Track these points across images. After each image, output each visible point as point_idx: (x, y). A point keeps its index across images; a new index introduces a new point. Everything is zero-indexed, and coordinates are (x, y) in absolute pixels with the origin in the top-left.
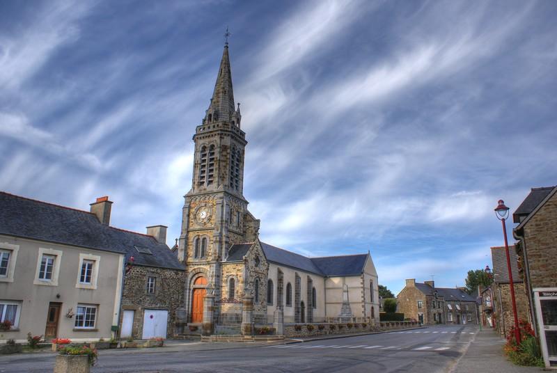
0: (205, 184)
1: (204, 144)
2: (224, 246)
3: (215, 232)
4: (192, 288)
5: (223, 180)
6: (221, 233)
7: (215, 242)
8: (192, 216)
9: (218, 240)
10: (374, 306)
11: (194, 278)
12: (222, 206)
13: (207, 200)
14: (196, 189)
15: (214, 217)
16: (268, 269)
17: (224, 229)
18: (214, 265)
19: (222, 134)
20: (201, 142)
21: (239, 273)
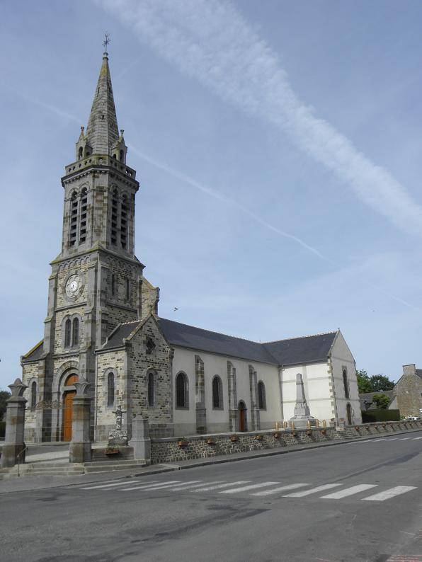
0: (76, 243)
1: (74, 189)
2: (99, 327)
3: (88, 308)
4: (62, 392)
5: (99, 235)
6: (94, 310)
7: (87, 322)
8: (60, 290)
9: (90, 318)
10: (351, 403)
11: (65, 377)
12: (96, 271)
13: (78, 266)
14: (65, 251)
15: (86, 288)
16: (172, 357)
17: (98, 303)
18: (85, 355)
19: (95, 172)
20: (70, 187)
21: (119, 365)
